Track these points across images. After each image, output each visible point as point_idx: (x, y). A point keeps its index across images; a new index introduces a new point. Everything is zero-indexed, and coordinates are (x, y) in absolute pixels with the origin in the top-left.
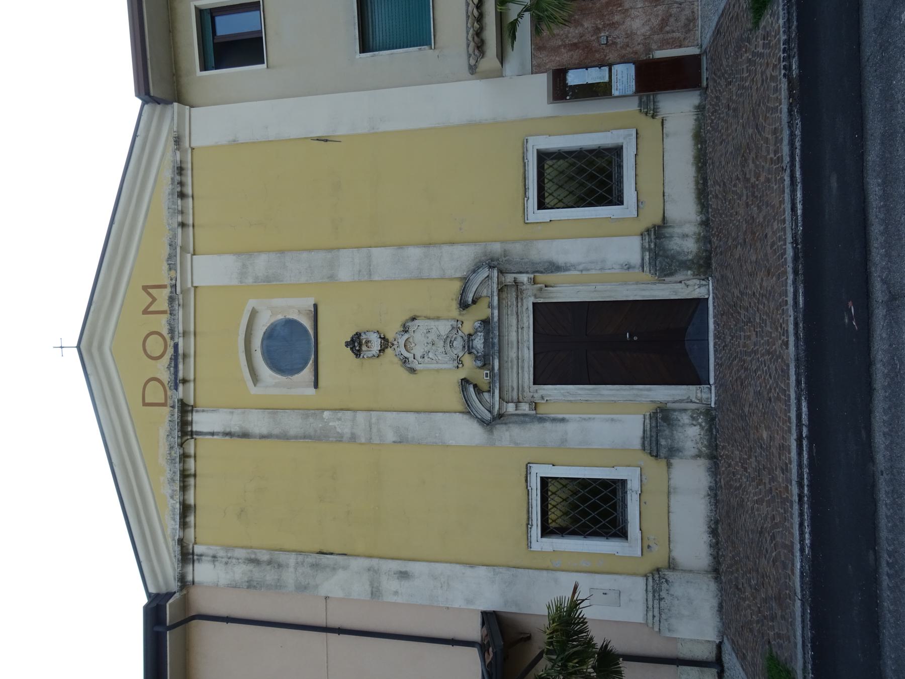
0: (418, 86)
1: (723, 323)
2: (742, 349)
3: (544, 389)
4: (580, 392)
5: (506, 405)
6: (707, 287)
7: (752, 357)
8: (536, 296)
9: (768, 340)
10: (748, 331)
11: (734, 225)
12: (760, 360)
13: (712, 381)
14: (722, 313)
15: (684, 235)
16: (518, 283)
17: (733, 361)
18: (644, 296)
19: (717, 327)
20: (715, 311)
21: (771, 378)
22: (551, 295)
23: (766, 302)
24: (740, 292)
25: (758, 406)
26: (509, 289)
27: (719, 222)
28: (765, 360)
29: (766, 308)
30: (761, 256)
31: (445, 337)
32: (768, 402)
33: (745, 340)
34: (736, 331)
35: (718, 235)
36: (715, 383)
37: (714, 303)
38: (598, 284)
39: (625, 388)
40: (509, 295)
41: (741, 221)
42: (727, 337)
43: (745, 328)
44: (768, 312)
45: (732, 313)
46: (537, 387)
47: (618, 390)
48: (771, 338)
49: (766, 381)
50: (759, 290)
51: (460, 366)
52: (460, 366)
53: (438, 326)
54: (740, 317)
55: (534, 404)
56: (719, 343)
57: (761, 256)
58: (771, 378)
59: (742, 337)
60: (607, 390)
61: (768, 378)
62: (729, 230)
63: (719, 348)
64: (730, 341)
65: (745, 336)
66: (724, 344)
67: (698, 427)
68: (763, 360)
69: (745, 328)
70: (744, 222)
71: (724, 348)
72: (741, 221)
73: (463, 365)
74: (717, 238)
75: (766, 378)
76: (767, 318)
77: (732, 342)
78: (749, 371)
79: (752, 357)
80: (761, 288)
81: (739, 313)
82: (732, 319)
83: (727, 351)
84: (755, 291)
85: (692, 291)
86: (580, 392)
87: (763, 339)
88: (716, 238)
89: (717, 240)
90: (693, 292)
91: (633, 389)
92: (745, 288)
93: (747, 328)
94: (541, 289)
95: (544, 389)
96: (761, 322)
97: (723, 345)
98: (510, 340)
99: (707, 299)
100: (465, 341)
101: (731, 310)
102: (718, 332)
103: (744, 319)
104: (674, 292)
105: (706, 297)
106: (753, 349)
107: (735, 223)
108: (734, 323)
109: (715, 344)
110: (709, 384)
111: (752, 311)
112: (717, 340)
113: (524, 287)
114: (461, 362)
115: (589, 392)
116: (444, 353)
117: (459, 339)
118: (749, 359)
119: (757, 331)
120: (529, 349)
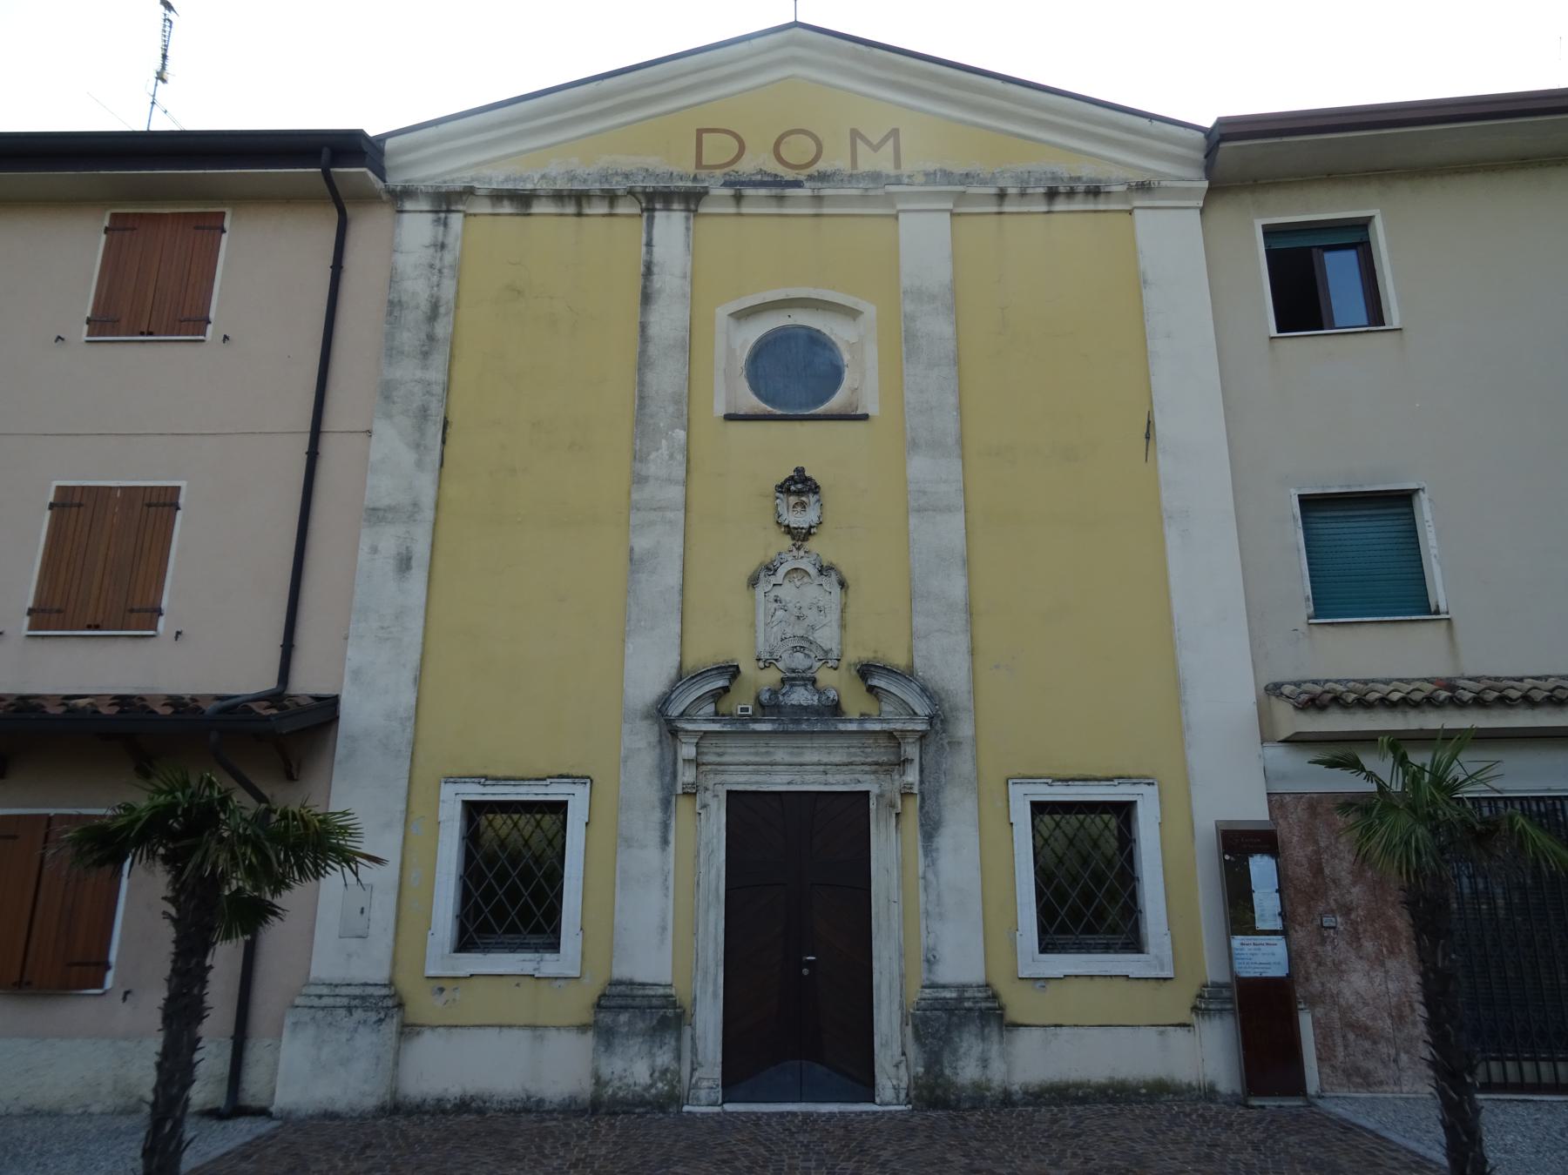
2: (785, 1164)
3: (719, 809)
4: (713, 872)
6: (895, 1101)
8: (880, 796)
13: (729, 1107)
15: (986, 1060)
16: (904, 765)
17: (765, 1146)
20: (853, 1115)
22: (882, 824)
31: (811, 638)
34: (818, 1153)
36: (725, 1113)
45: (848, 1146)
46: (723, 797)
54: (842, 1161)
55: (694, 791)
65: (809, 1168)
67: (649, 1081)
86: (713, 872)
95: (719, 809)
98: (804, 750)
99: (873, 1101)
100: (804, 672)
109: (794, 1114)
110: (724, 1102)
112: (800, 1118)
113: (897, 777)
114: (767, 665)
117: (807, 663)
120: (788, 783)
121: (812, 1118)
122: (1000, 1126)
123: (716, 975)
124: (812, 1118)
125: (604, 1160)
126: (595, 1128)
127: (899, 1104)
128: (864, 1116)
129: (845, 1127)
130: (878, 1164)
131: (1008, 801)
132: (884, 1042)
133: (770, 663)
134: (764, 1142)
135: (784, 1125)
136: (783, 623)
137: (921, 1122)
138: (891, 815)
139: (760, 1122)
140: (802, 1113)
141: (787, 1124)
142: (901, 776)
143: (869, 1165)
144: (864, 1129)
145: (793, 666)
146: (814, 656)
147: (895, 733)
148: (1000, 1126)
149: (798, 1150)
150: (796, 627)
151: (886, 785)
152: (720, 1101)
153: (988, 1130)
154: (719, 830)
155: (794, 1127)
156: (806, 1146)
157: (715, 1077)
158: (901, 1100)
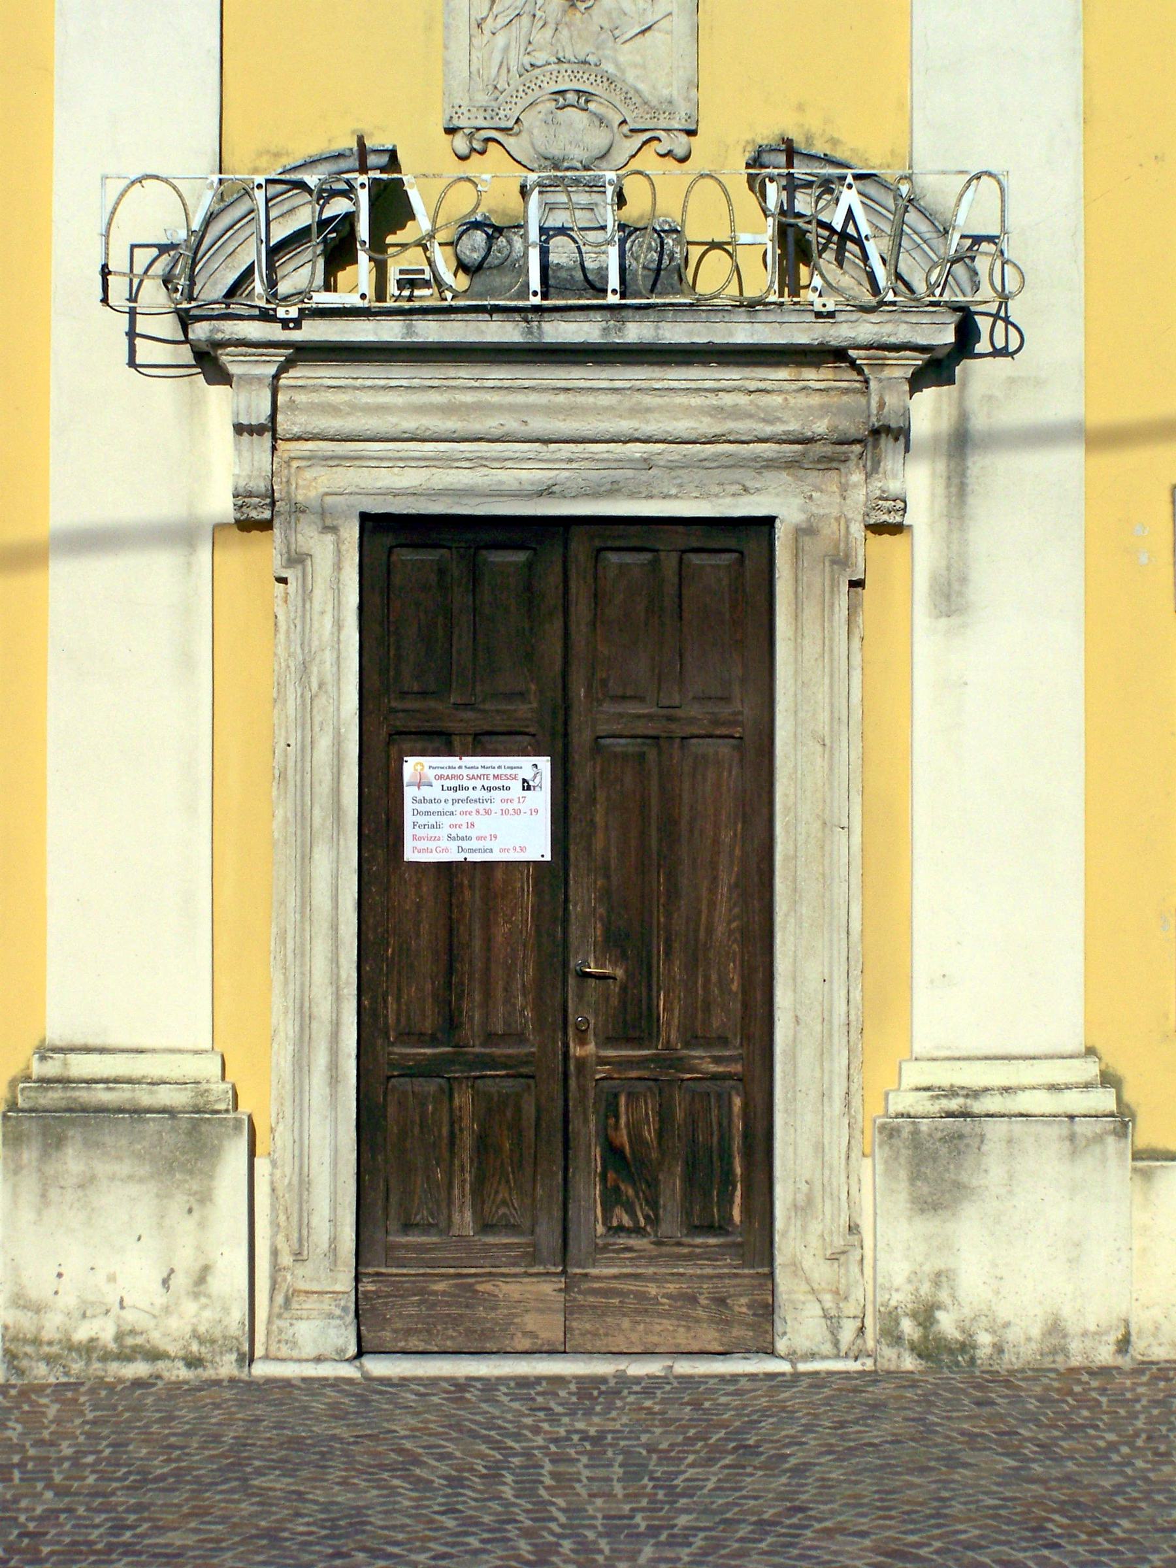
0: (355, 1116)
1: (657, 1408)
2: (544, 1472)
3: (338, 567)
4: (324, 743)
5: (259, 379)
6: (827, 1348)
7: (518, 1501)
8: (806, 531)
9: (600, 1552)
10: (630, 1491)
11: (1113, 1447)
12: (509, 1527)
13: (378, 1367)
14: (707, 1404)
15: (1078, 1245)
16: (876, 445)
17: (487, 1440)
18: (793, 1057)
19: (636, 1388)
20: (712, 1381)
21: (434, 1558)
22: (811, 611)
23: (763, 1546)
24: (804, 1464)
25: (301, 1520)
26: (532, 151)
27: (1129, 1395)
28: (509, 1540)
29: (736, 1545)
30: (965, 1532)
31: (610, 68)
32: (330, 1551)
33: (589, 1479)
34: (626, 1452)
35: (1071, 1393)
36: (368, 1378)
37: (752, 1377)
38: (856, 840)
39: (343, 960)
40: (816, 400)
41: (1129, 1471)
42: (596, 1420)
43: (645, 1481)
44: (723, 1552)
45: (706, 1439)
46: (351, 533)
47: (335, 928)
48: (607, 1559)
49: (418, 1544)
50: (817, 1526)
51: (461, 143)
52: (462, 147)
53: (670, 33)
54: (691, 1466)
55: (267, 515)
56: (563, 1393)
57: (965, 1532)
58: (434, 1558)
59: (601, 1472)
60: (336, 876)
61: (430, 1549)
62: (1091, 1432)
63: (538, 1394)
64: (577, 1432)
65: (608, 1479)
66: (559, 1409)
67: (160, 1298)
68: (509, 1535)
69: (645, 1481)
70: (1120, 1479)
71: (540, 1409)
72: (1129, 1471)
73: (463, 158)
74: (1058, 1390)
75: (431, 1545)
76: (693, 1549)
77: (576, 1437)
78: (449, 1491)
79: (518, 1501)
80: (826, 1530)
81: (710, 1461)
82: (680, 1438)
83: (528, 1421)
84: (810, 1513)
85: (808, 1281)
86: (324, 743)
87: (600, 1535)
88: (1056, 1384)
89: (1047, 1388)
90: (804, 1287)
91: (338, 998)
92: (823, 1479)
93: (645, 1487)
94: (840, 560)
95: (338, 567)
96: (676, 1531)
97: (552, 1405)
98: (217, 274)
99: (772, 1353)
100: (587, 168)
101: (722, 1433)
102: (617, 1393)
103: (682, 1477)
104: (810, 1200)
105: (781, 1346)
106: (554, 1504)
107: (1118, 1451)
108: (664, 1446)
109: (558, 1381)
110: (360, 1354)
111: (720, 1501)
112: (573, 1387)
113: (857, 477)
114: (477, 145)
115: (324, 788)
116: (527, 60)
117: (598, 140)
118: (508, 1492)
119: (632, 1518)
120: (540, 494)
121: (603, 1388)
122: (1104, 1400)
123: (336, 1025)
124: (603, 1388)
125: (72, 1465)
126: (26, 1407)
127: (837, 1356)
128: (743, 1381)
129: (697, 1405)
130: (786, 1471)
131: (332, 440)
132: (801, 1199)
133: (488, 140)
134: (484, 1432)
135: (533, 1399)
136: (525, 20)
137: (895, 1393)
138: (834, 585)
139: (468, 1395)
140: (576, 1377)
141: (540, 1399)
142: (868, 476)
143: (760, 1473)
144: (744, 1407)
145: (555, 151)
146: (618, 119)
147: (852, 353)
148: (1104, 1400)
149: (574, 1446)
150: (564, 33)
151: (825, 498)
152: (352, 1350)
153: (1072, 1407)
154: (338, 625)
155: (561, 1404)
156: (598, 1440)
157: (338, 1288)
158: (844, 1347)
